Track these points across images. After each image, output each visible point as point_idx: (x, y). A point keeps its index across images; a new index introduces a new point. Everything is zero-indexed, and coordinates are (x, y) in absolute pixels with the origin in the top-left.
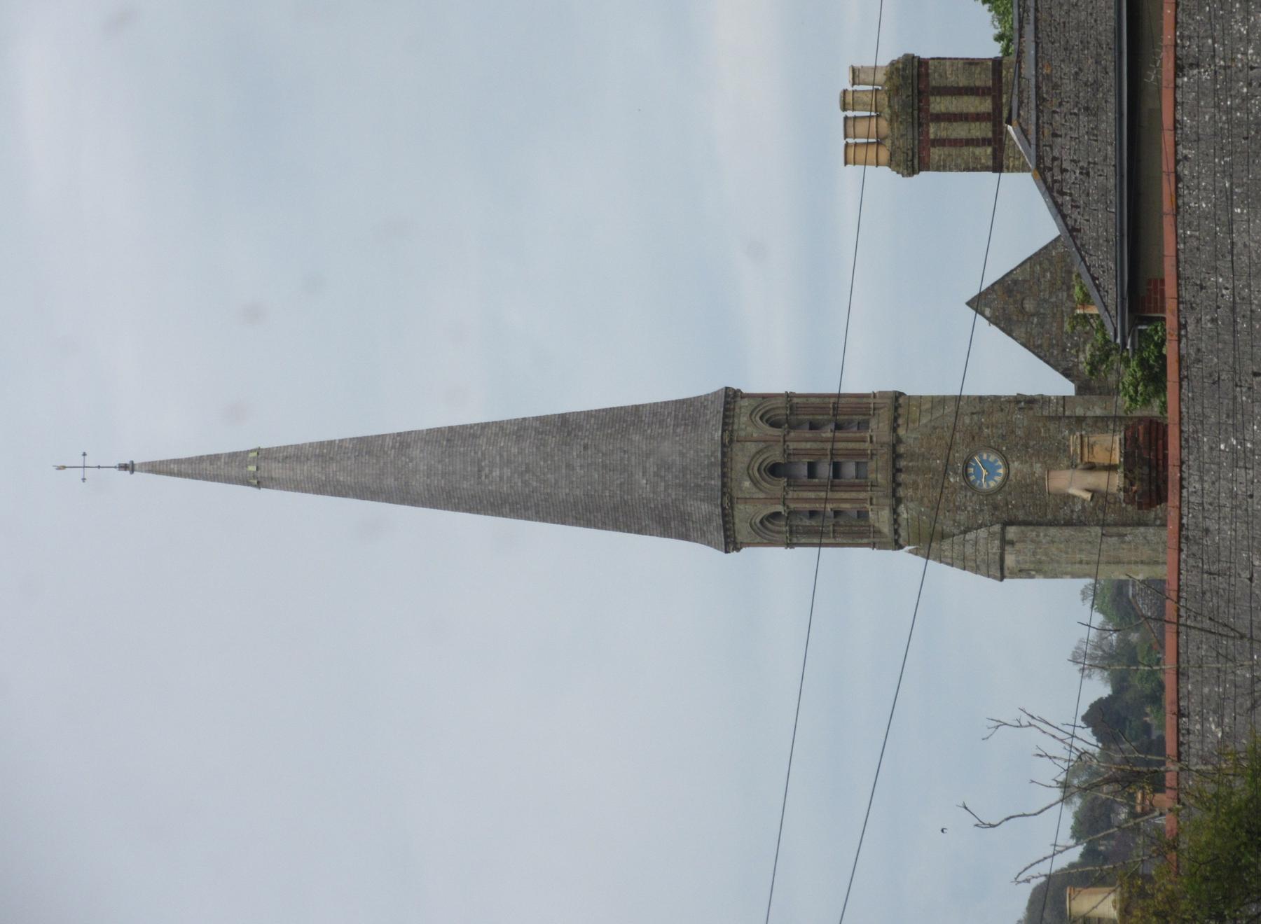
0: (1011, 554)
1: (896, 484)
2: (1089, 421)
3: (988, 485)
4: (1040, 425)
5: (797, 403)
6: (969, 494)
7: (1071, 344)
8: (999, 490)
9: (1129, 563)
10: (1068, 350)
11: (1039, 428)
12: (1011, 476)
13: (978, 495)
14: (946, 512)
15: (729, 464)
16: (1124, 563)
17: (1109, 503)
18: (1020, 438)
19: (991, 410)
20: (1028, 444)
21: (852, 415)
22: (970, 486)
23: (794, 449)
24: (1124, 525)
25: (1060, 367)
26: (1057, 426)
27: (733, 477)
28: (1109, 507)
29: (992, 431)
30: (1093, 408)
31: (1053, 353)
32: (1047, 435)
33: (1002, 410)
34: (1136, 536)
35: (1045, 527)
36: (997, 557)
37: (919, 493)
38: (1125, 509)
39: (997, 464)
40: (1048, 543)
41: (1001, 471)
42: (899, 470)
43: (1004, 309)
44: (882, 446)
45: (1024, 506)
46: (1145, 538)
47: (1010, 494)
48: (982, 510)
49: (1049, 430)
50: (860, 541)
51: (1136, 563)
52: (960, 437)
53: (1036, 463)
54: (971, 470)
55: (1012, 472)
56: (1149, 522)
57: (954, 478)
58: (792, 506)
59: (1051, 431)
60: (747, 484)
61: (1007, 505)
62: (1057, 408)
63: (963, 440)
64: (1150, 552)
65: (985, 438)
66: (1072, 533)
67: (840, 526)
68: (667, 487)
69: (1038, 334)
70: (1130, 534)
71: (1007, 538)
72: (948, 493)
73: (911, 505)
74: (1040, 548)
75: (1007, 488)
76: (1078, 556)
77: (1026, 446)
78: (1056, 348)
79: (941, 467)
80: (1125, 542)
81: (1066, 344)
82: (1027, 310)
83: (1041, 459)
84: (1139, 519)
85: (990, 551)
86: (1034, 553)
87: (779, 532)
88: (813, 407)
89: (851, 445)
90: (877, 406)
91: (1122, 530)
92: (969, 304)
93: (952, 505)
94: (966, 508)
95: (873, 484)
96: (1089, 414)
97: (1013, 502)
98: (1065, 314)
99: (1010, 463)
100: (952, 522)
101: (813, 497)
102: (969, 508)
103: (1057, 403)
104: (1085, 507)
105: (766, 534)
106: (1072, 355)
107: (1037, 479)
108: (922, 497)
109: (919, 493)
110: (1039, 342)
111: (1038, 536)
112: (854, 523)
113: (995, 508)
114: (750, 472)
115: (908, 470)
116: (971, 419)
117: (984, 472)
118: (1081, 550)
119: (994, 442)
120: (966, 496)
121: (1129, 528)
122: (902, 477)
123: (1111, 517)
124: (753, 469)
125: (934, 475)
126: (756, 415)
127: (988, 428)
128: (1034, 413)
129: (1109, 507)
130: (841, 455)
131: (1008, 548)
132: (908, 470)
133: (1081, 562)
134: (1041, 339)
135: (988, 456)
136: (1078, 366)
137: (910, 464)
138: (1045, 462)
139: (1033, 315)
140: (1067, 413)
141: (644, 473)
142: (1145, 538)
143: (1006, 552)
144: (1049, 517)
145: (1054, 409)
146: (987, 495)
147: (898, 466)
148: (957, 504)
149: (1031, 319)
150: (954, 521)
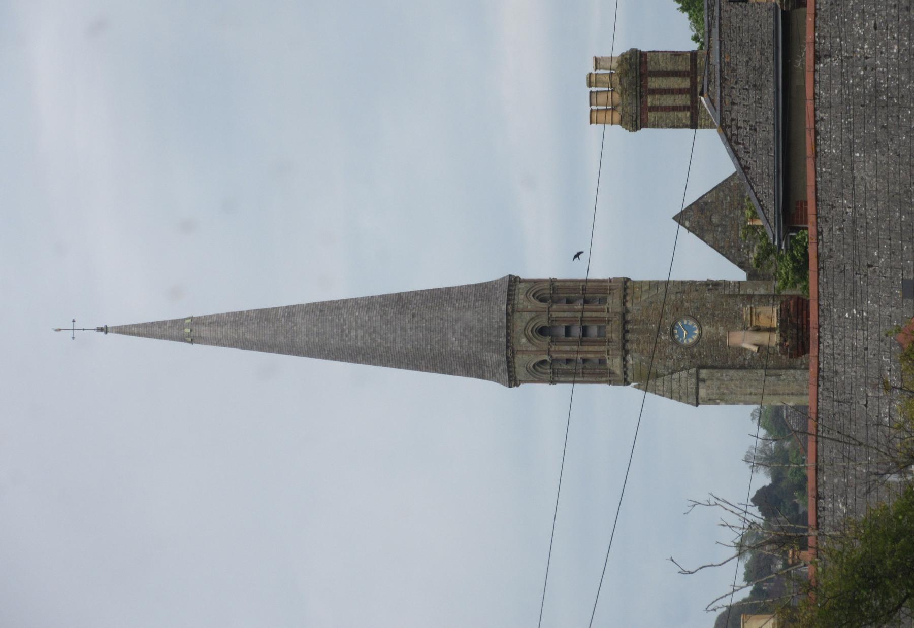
0: (703, 388)
1: (625, 341)
2: (757, 298)
3: (687, 341)
4: (723, 300)
6: (675, 347)
7: (744, 245)
15: (512, 327)
22: (675, 342)
23: (556, 317)
26: (734, 301)
28: (770, 357)
33: (697, 290)
35: (726, 370)
36: (694, 391)
38: (781, 357)
41: (696, 332)
45: (712, 355)
46: (794, 377)
51: (788, 394)
54: (676, 331)
56: (797, 367)
59: (731, 304)
60: (524, 340)
61: (700, 354)
64: (798, 387)
68: (469, 342)
69: (722, 239)
70: (784, 374)
71: (700, 377)
74: (723, 384)
75: (700, 343)
77: (713, 315)
82: (714, 223)
86: (719, 388)
89: (594, 314)
90: (612, 287)
91: (778, 372)
93: (663, 355)
96: (756, 293)
97: (705, 353)
98: (740, 225)
100: (663, 367)
101: (569, 349)
102: (675, 357)
103: (735, 286)
110: (722, 244)
113: (692, 357)
118: (751, 386)
120: (672, 349)
127: (687, 302)
128: (719, 292)
131: (701, 385)
133: (751, 394)
135: (688, 322)
136: (749, 260)
137: (635, 327)
142: (794, 377)
144: (730, 363)
148: (666, 354)
150: (665, 365)
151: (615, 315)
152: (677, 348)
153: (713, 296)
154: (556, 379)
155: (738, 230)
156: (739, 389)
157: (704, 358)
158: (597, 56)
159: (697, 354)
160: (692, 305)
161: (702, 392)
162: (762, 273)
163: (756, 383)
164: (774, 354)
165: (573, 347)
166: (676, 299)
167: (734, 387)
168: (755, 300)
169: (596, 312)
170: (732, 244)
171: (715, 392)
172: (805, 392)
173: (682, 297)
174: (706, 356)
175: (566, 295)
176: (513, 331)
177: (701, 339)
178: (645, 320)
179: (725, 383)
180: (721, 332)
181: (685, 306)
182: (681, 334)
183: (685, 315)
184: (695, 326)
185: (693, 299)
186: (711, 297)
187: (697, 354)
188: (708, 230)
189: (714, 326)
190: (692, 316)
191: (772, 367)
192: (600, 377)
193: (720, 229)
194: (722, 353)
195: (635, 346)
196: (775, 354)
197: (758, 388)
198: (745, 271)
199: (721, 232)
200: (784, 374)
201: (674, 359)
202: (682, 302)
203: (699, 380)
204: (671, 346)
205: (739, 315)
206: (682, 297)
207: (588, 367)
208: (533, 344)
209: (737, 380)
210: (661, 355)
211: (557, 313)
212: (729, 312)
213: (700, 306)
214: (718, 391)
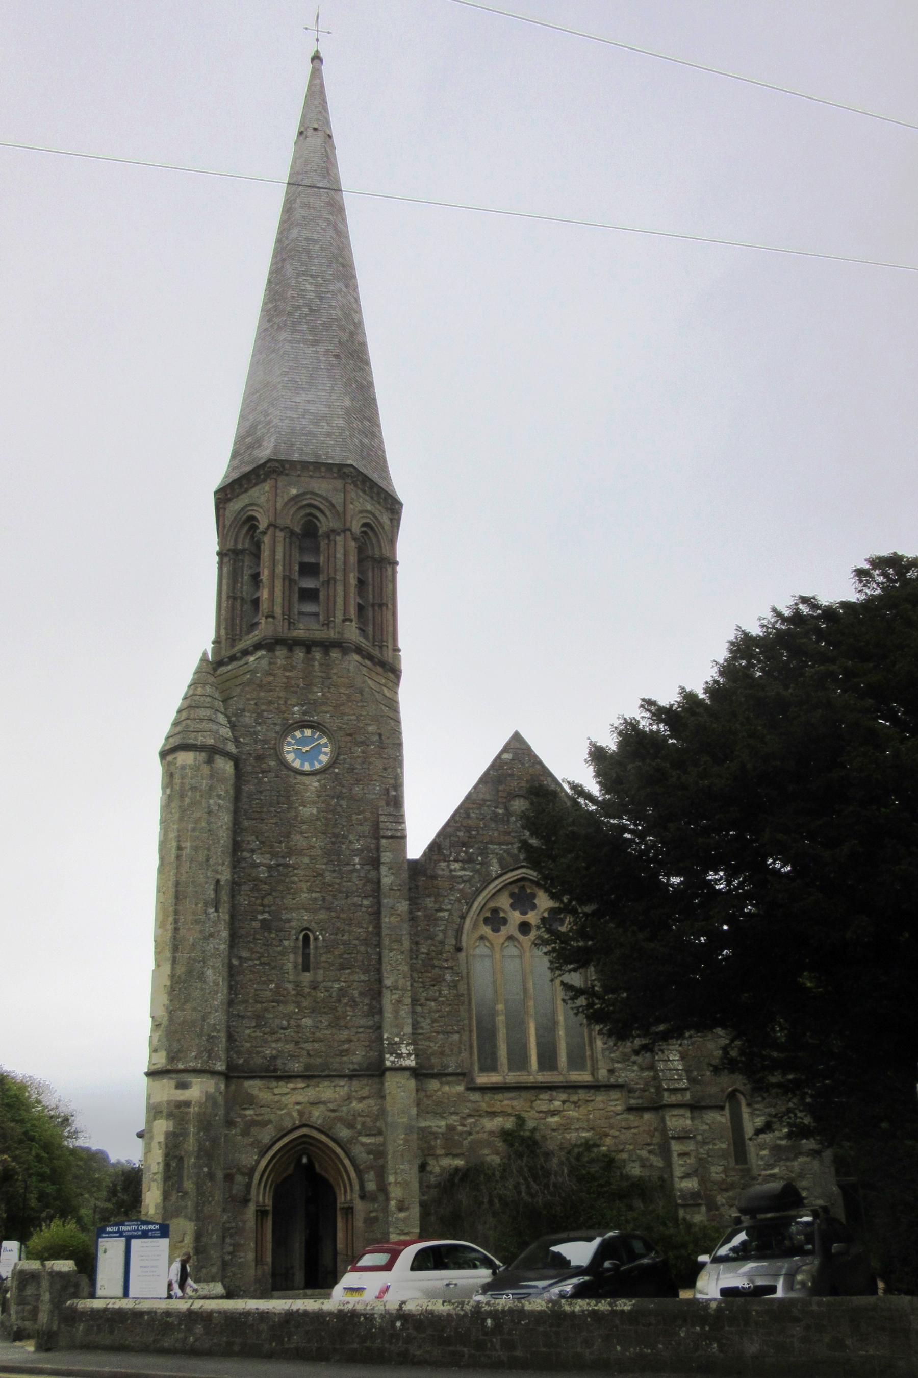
0: (195, 759)
1: (291, 644)
2: (373, 874)
3: (288, 752)
4: (368, 814)
5: (386, 570)
6: (278, 728)
7: (472, 853)
8: (282, 763)
9: (176, 912)
10: (464, 849)
11: (363, 812)
12: (299, 777)
13: (276, 739)
14: (255, 701)
15: (317, 474)
16: (176, 905)
17: (263, 898)
18: (351, 789)
19: (385, 756)
20: (343, 799)
21: (374, 625)
22: (288, 729)
23: (335, 542)
24: (232, 916)
25: (441, 839)
26: (366, 834)
27: (303, 479)
28: (257, 898)
29: (359, 757)
30: (393, 874)
31: (460, 831)
32: (354, 822)
33: (385, 769)
34: (215, 924)
35: (232, 809)
36: (191, 741)
37: (279, 672)
38: (254, 919)
39: (316, 763)
40: (209, 807)
41: (307, 767)
42: (308, 651)
43: (512, 775)
44: (339, 633)
45: (261, 792)
46: (211, 935)
47: (277, 777)
48: (256, 742)
49: (361, 825)
50: (223, 627)
51: (176, 921)
52: (351, 720)
53: (317, 808)
54: (308, 732)
55: (305, 779)
56: (235, 950)
57: (299, 711)
58: (267, 539)
59: (360, 827)
60: (294, 491)
61: (263, 772)
62: (391, 830)
63: (347, 723)
64: (191, 940)
65: (350, 749)
66: (222, 842)
67: (242, 606)
68: (292, 419)
69: (481, 814)
70: (219, 916)
71: (217, 757)
72: (278, 704)
73: (264, 663)
74: (202, 796)
75: (285, 772)
76: (188, 844)
77: (339, 796)
78: (467, 835)
79: (314, 698)
80: (206, 906)
81: (472, 847)
82: (512, 803)
83: (322, 814)
84: (240, 937)
85: (200, 734)
86: (193, 788)
87: (236, 541)
88: (382, 622)
89: (340, 601)
90: (385, 648)
91: (225, 908)
92: (517, 737)
93: (264, 707)
94: (260, 724)
95: (292, 624)
96: (384, 870)
97: (266, 779)
98: (510, 846)
99: (318, 777)
100: (241, 707)
101: (277, 557)
102: (259, 728)
103: (396, 830)
104: (259, 867)
105: (258, 1188)
106: (458, 854)
107: (296, 808)
108: (274, 675)
109: (279, 672)
110: (473, 815)
111: (219, 797)
112: (245, 620)
113: (260, 758)
114: (308, 496)
115: (309, 661)
116: (373, 734)
117: (305, 749)
118: (196, 849)
119: (345, 759)
120: (275, 724)
121: (227, 917)
122: (300, 654)
123: (243, 901)
124: (311, 498)
125: (303, 688)
126: (364, 517)
127: (363, 752)
128: (382, 807)
129: (257, 898)
130: (328, 594)
131: (202, 756)
132: (309, 661)
133: (179, 848)
134: (477, 818)
135: (326, 754)
136: (445, 861)
137: (316, 663)
138: (317, 819)
139: (506, 809)
140: (383, 841)
141: (308, 402)
142: (211, 935)
143: (198, 753)
144: (246, 823)
145: (390, 827)
146: (275, 749)
147: (314, 649)
148: (265, 714)
149: (501, 806)
150: (243, 710)
151: (339, 633)
152: (277, 733)
153: (374, 796)
154: (226, 560)
155: (500, 844)
156: (190, 826)
157: (257, 778)
158: (639, 705)
159: (264, 766)
160: (359, 760)
161: (186, 758)
162: (419, 884)
163: (201, 858)
164: (262, 905)
165: (281, 563)
166: (368, 733)
167: (194, 816)
168: (369, 871)
169: (345, 604)
170: (474, 833)
171: (186, 781)
172: (178, 955)
173: (373, 743)
174: (260, 781)
175: (370, 580)
176: (311, 477)
177: (292, 774)
178: (330, 681)
179: (204, 801)
180: (305, 809)
181: (356, 748)
182: (303, 741)
183: (339, 748)
184: (317, 766)
185: (370, 763)
186: (375, 794)
187: (264, 766)
188: (498, 791)
189: (318, 797)
190: (337, 759)
191: (236, 902)
192: (227, 625)
193: (500, 811)
194: (265, 810)
195: (280, 662)
196: (260, 908)
197: (191, 863)
198: (425, 854)
199: (496, 814)
200: (219, 916)
201: (255, 727)
202: (363, 743)
203: (212, 752)
204: (279, 721)
205: (340, 842)
206: (373, 743)
207: (245, 607)
208: (286, 504)
209: (209, 823)
210: (263, 704)
211: (342, 543)
212: (345, 824)
213: (357, 774)
214: (187, 787)
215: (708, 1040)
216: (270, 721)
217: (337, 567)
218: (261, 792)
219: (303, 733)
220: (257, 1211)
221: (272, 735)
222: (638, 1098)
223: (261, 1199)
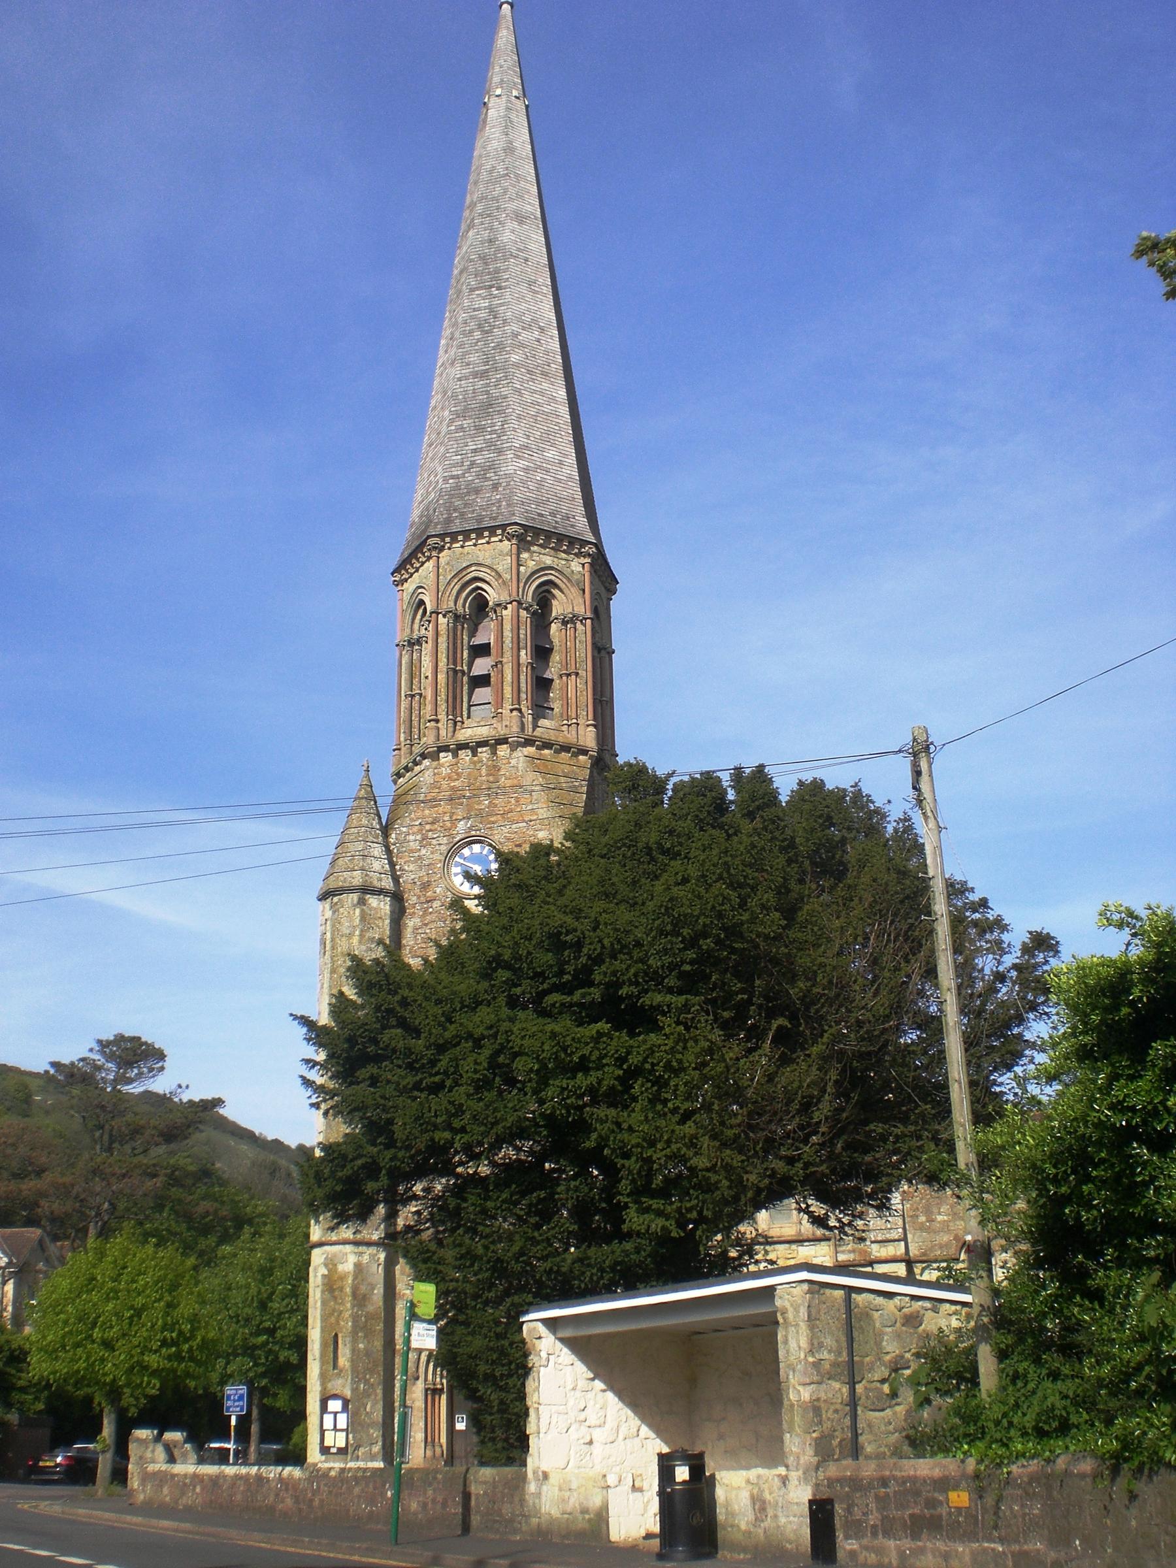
102: (423, 851)
195: (445, 771)
215: (872, 1206)
216: (434, 842)
217: (858, 1395)
218: (426, 925)
219: (471, 849)
220: (427, 1390)
221: (437, 856)
222: (850, 1252)
223: (430, 1377)
